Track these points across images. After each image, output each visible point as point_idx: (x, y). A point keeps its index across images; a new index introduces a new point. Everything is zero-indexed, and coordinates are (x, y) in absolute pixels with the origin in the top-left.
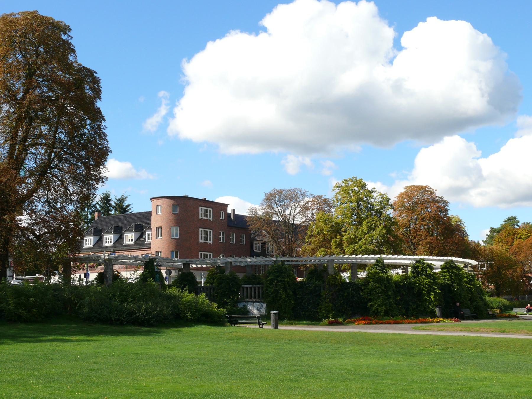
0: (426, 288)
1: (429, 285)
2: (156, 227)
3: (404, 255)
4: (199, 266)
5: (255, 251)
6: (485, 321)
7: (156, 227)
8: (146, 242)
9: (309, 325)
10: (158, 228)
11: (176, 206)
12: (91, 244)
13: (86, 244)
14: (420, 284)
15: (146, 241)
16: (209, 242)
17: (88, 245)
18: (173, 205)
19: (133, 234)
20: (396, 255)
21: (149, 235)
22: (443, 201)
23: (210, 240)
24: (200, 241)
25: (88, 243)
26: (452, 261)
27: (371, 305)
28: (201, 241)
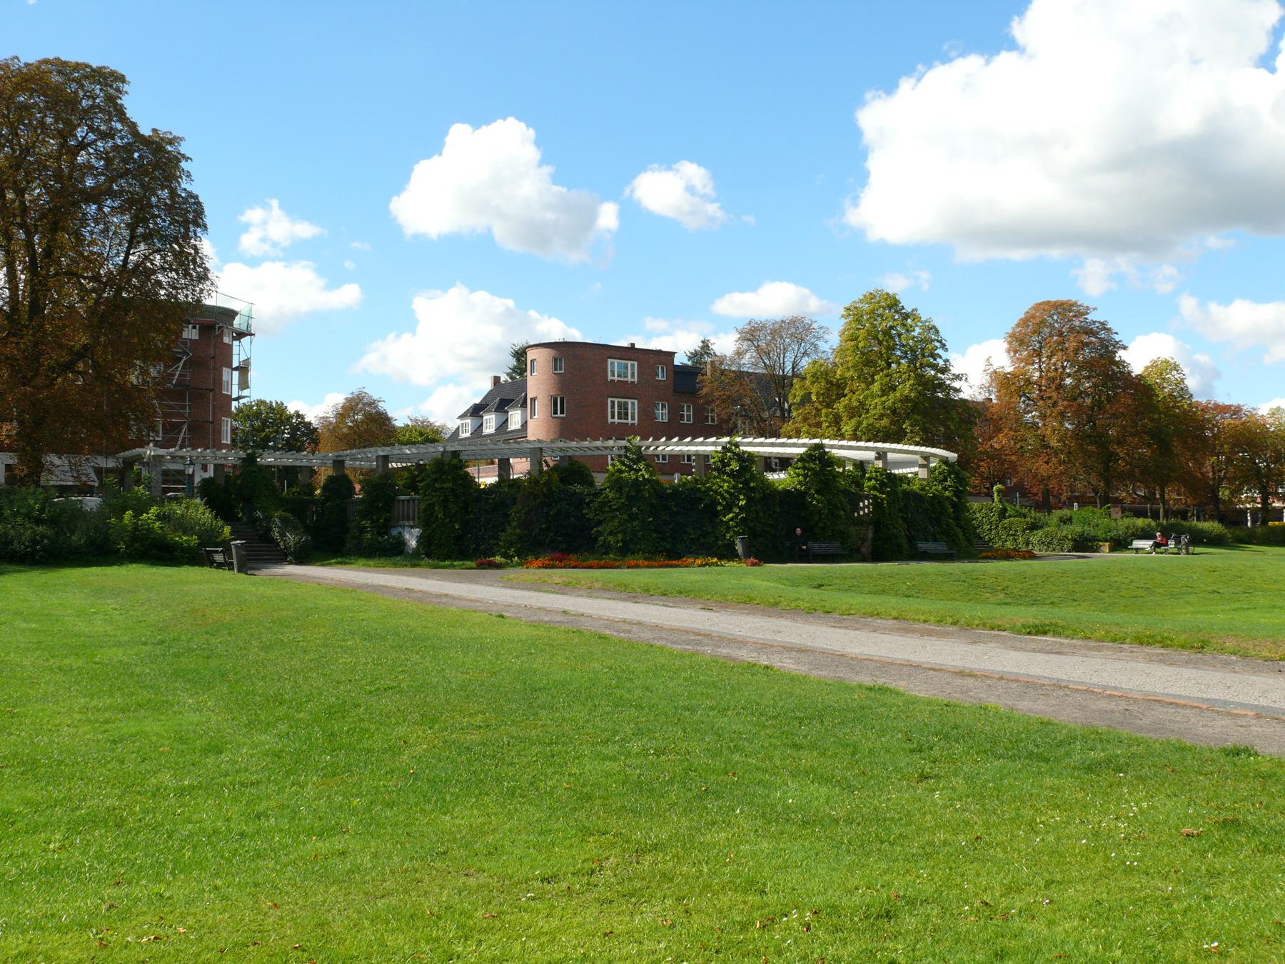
0: (724, 498)
1: (731, 494)
3: (778, 437)
4: (404, 465)
6: (844, 565)
9: (435, 568)
11: (561, 360)
14: (715, 492)
16: (630, 421)
18: (555, 360)
19: (520, 412)
20: (761, 437)
22: (1105, 329)
23: (633, 419)
24: (610, 420)
26: (821, 446)
27: (597, 531)
28: (613, 420)
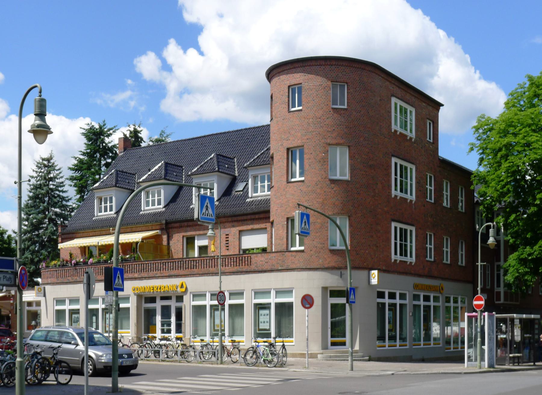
2: (288, 149)
5: (497, 302)
7: (288, 149)
8: (248, 200)
10: (290, 152)
12: (159, 204)
13: (147, 204)
15: (250, 195)
17: (153, 204)
21: (111, 207)
25: (153, 202)
